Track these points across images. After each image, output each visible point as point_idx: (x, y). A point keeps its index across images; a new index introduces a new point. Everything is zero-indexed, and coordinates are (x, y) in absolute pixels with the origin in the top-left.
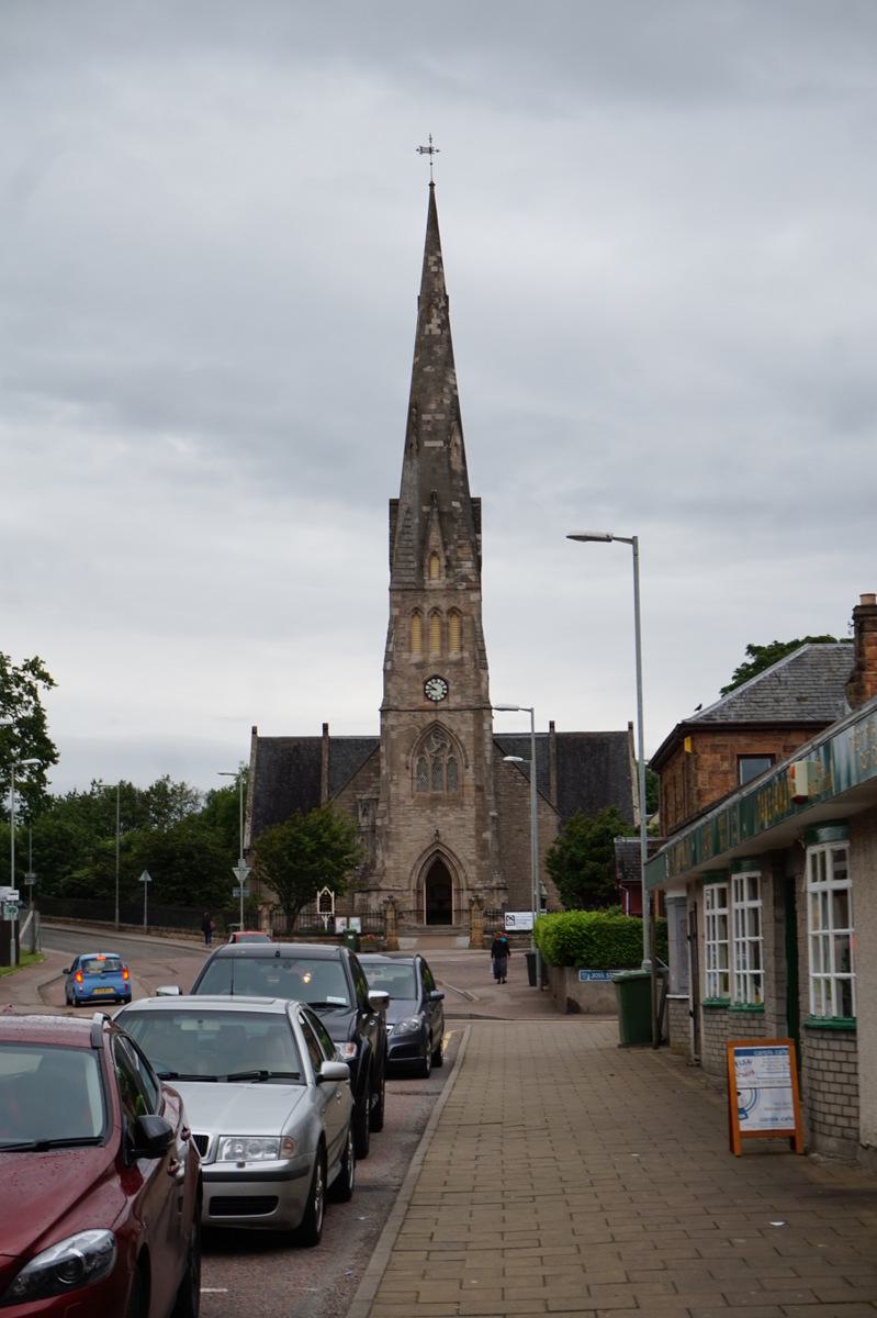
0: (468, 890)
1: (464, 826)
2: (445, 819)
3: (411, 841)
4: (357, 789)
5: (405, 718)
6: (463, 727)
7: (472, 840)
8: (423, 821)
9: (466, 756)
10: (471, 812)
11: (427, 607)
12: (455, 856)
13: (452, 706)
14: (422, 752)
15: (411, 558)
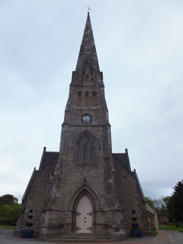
0: (100, 211)
1: (98, 177)
3: (71, 184)
7: (102, 184)
8: (78, 174)
9: (99, 145)
11: (84, 91)
12: (93, 192)
13: (93, 124)
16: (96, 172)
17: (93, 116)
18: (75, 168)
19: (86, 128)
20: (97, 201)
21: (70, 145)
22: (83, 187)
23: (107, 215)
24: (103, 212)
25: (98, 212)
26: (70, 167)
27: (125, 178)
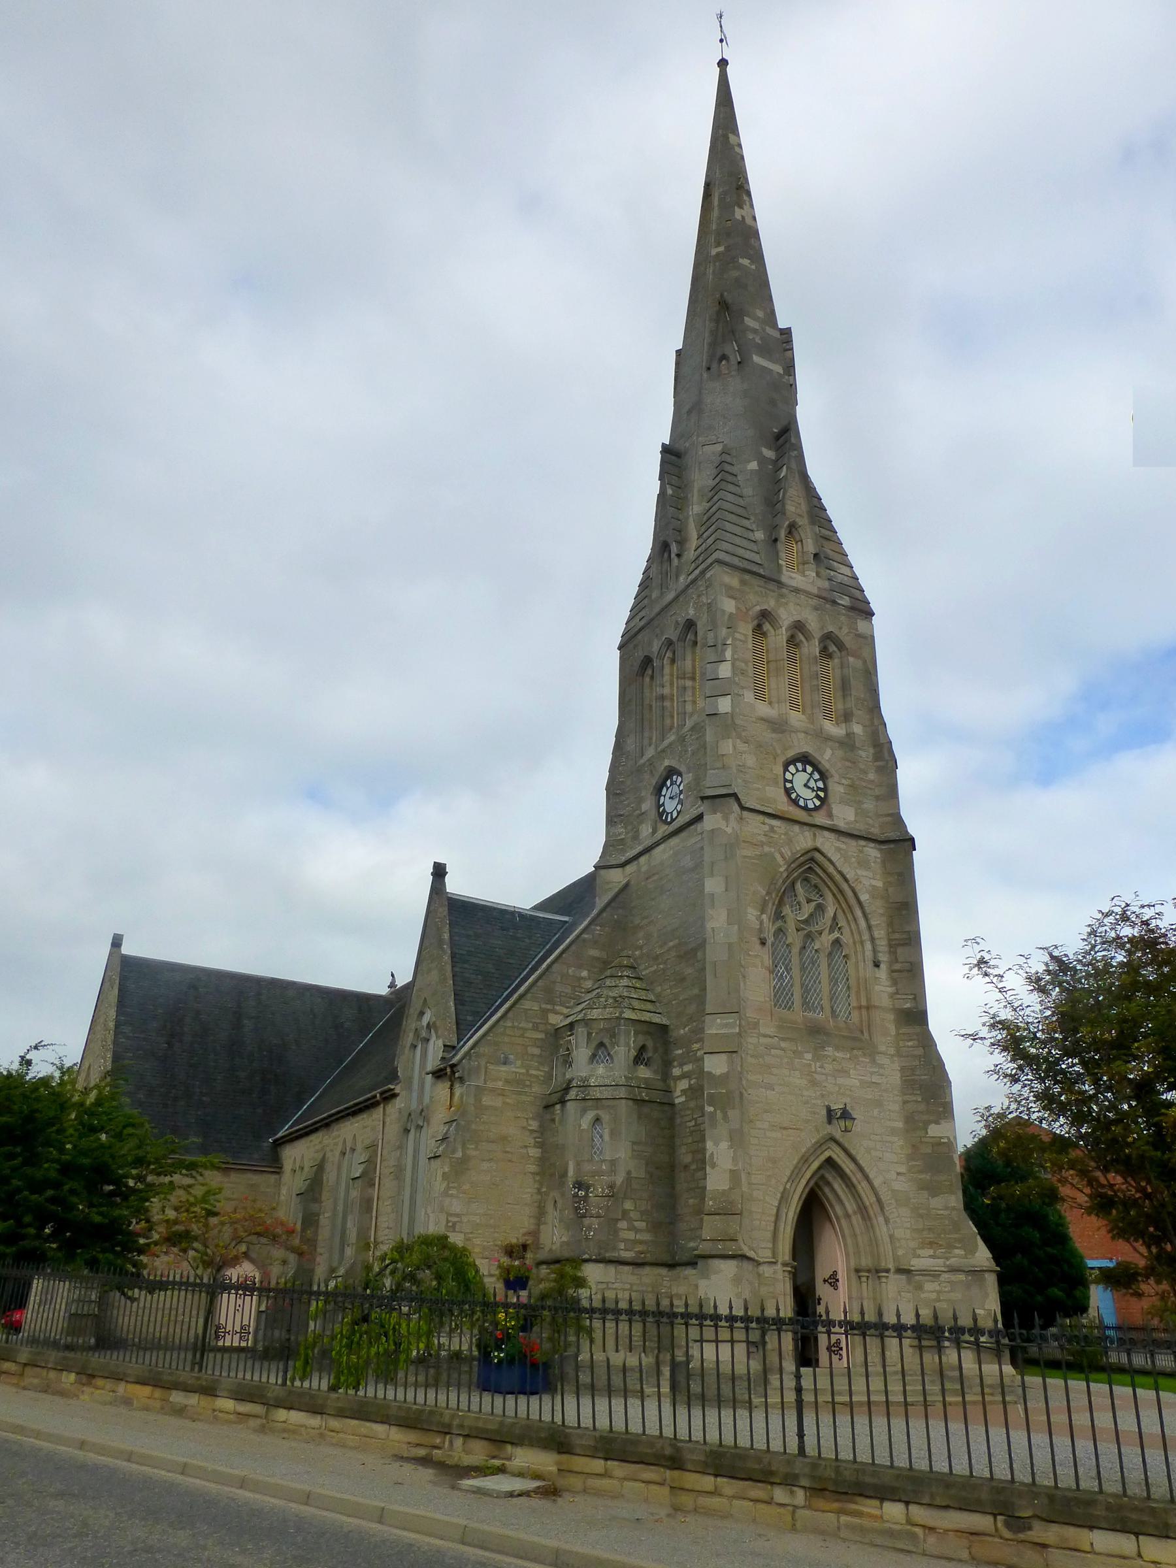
0: (900, 1271)
1: (878, 1103)
2: (840, 1081)
4: (550, 1001)
5: (755, 826)
6: (863, 871)
7: (898, 1142)
8: (798, 1080)
9: (873, 939)
12: (867, 1177)
14: (778, 916)
16: (867, 1079)
17: (836, 778)
18: (783, 1044)
19: (815, 835)
20: (881, 1219)
21: (749, 917)
22: (824, 1147)
23: (929, 1286)
24: (907, 1272)
25: (891, 1275)
26: (762, 1040)
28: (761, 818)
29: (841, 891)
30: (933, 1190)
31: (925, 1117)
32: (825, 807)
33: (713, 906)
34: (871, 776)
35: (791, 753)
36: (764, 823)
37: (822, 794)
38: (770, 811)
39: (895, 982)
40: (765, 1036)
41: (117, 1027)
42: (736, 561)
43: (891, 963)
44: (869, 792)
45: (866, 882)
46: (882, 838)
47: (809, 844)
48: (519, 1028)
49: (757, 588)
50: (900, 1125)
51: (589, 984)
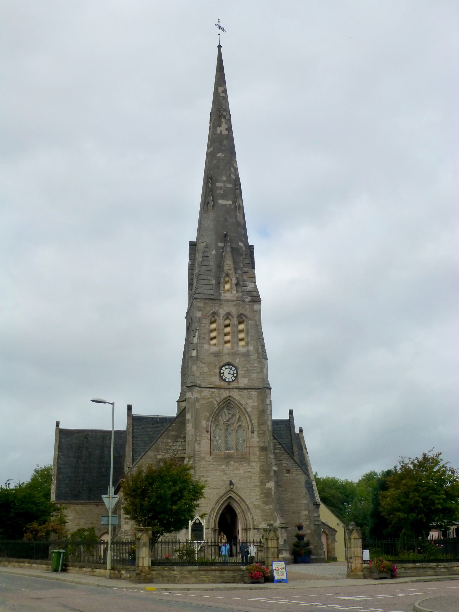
0: (254, 529)
1: (250, 478)
2: (235, 472)
4: (158, 452)
5: (206, 393)
6: (250, 402)
7: (257, 489)
10: (256, 467)
11: (222, 312)
12: (244, 501)
13: (241, 385)
15: (210, 277)
18: (214, 463)
20: (249, 514)
25: (252, 530)
26: (206, 463)
27: (288, 471)
28: (209, 389)
29: (241, 409)
30: (266, 503)
31: (266, 481)
32: (237, 379)
33: (188, 423)
34: (256, 365)
35: (222, 364)
36: (210, 391)
37: (235, 375)
38: (212, 386)
39: (259, 437)
40: (207, 461)
41: (58, 457)
42: (203, 296)
43: (258, 431)
44: (254, 371)
45: (250, 404)
46: (258, 387)
47: (228, 395)
48: (147, 461)
49: (211, 304)
50: (258, 484)
51: (171, 444)
